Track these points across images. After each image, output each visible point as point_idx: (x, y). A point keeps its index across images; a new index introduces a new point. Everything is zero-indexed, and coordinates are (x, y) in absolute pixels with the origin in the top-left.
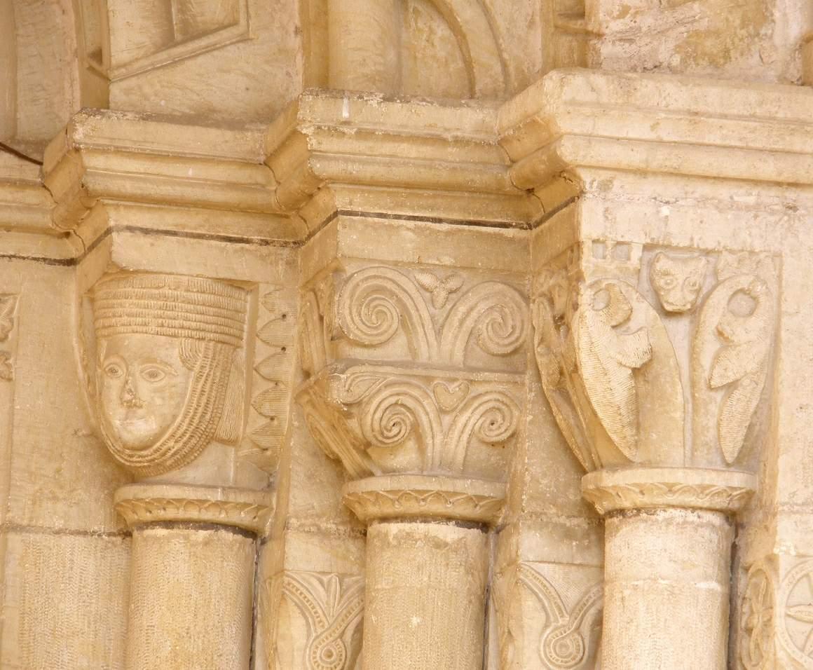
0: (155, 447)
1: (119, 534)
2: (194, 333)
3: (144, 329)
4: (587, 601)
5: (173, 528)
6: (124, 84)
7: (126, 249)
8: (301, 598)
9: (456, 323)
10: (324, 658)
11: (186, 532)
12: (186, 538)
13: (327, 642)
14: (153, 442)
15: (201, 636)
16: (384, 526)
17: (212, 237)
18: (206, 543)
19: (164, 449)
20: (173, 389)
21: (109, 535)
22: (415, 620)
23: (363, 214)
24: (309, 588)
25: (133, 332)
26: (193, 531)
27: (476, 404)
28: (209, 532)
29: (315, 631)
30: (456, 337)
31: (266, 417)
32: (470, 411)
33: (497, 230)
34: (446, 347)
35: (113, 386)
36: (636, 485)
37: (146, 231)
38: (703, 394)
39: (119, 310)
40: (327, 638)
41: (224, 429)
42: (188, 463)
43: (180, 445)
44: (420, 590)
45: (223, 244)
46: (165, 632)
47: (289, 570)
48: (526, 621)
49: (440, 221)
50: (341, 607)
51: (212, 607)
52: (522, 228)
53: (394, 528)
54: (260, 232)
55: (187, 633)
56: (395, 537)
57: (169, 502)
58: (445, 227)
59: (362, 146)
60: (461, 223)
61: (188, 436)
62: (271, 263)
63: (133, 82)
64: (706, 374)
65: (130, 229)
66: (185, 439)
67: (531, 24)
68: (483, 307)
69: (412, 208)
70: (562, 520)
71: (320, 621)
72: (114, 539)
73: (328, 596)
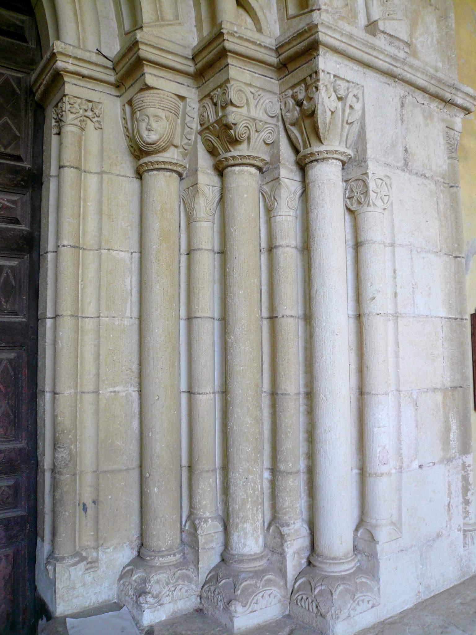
6: (148, 29)
7: (150, 80)
12: (164, 174)
14: (157, 142)
16: (233, 168)
17: (174, 81)
18: (170, 176)
23: (236, 66)
30: (260, 109)
35: (143, 125)
36: (326, 151)
37: (155, 76)
38: (345, 124)
39: (146, 101)
41: (175, 143)
49: (256, 73)
53: (237, 168)
56: (238, 171)
57: (160, 162)
58: (257, 75)
59: (239, 41)
63: (150, 29)
64: (346, 119)
65: (150, 74)
67: (275, 22)
68: (267, 101)
70: (290, 166)
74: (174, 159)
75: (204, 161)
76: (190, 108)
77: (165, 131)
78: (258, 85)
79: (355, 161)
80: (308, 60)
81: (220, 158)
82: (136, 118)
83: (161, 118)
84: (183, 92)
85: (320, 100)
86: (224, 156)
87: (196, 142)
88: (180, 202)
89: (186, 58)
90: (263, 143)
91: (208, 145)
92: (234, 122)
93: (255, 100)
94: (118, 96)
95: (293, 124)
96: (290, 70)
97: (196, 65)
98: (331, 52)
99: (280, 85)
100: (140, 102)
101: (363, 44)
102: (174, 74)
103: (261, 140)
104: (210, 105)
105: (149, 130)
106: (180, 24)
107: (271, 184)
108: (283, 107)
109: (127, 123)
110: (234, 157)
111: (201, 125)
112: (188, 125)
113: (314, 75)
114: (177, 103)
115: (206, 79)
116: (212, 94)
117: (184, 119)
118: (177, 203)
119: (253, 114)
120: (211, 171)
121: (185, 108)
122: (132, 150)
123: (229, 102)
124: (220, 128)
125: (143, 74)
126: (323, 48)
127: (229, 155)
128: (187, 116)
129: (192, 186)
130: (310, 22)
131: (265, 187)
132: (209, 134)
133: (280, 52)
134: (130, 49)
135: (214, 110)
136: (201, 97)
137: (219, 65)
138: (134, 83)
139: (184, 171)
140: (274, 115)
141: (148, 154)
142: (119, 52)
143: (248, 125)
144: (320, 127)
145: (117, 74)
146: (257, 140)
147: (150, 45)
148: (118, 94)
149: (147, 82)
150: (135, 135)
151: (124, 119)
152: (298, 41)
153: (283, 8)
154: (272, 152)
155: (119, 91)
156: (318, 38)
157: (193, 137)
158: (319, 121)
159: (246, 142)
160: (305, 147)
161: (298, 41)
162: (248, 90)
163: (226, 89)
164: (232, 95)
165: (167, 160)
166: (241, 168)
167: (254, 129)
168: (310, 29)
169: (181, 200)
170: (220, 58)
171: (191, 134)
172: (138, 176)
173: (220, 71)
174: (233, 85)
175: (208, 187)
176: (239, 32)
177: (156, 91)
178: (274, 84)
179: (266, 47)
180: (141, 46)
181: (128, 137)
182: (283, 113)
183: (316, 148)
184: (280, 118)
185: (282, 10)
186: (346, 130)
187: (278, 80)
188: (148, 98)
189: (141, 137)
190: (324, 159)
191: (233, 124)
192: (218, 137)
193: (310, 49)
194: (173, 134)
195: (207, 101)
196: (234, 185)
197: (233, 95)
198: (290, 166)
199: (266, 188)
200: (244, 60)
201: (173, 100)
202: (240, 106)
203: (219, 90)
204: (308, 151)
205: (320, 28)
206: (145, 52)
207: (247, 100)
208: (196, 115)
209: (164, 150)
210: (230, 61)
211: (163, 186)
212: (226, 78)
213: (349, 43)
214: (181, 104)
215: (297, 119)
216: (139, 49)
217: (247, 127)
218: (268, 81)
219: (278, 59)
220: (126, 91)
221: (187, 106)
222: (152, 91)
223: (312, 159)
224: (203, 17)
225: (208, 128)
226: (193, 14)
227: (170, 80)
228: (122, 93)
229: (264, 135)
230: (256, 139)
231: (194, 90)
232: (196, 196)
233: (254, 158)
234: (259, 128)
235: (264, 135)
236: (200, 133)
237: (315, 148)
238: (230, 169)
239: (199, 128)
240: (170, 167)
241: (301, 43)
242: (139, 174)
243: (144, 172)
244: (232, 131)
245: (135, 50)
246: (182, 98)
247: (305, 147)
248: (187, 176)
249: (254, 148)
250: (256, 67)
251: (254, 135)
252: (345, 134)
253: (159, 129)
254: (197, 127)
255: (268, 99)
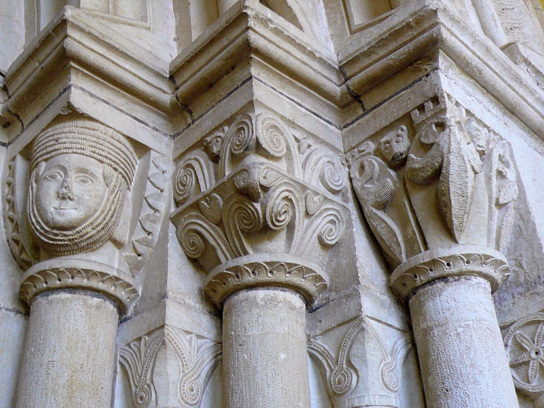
0: (77, 230)
1: (13, 311)
2: (113, 164)
3: (82, 151)
4: (397, 348)
5: (75, 294)
8: (175, 346)
9: (312, 164)
10: (188, 391)
11: (85, 297)
12: (85, 302)
13: (191, 380)
14: (79, 224)
15: (91, 371)
16: (252, 293)
17: (128, 114)
19: (84, 232)
20: (97, 192)
21: (7, 310)
22: (283, 356)
24: (180, 340)
25: (74, 153)
26: (90, 297)
27: (325, 214)
28: (101, 300)
29: (183, 371)
31: (146, 231)
32: (321, 218)
33: (326, 123)
34: (307, 176)
35: (51, 188)
37: (92, 95)
40: (191, 377)
42: (94, 250)
43: (95, 232)
44: (283, 336)
45: (134, 120)
46: (64, 366)
47: (168, 325)
48: (368, 356)
49: (301, 106)
50: (198, 357)
51: (99, 352)
52: (337, 128)
53: (261, 294)
54: (154, 122)
55: (82, 368)
56: (263, 299)
57: (79, 272)
60: (310, 111)
61: (101, 226)
62: (158, 141)
65: (82, 89)
66: (99, 228)
67: (327, 41)
68: (325, 159)
69: (288, 92)
71: (186, 365)
72: (9, 313)
73: (191, 348)
74: (113, 268)
75: (181, 281)
76: (157, 171)
77: (99, 204)
78: (307, 127)
79: (518, 285)
80: (410, 82)
81: (222, 269)
82: (37, 174)
83: (92, 174)
84: (144, 136)
85: (454, 146)
86: (232, 263)
87: (164, 239)
88: (115, 372)
89: (158, 75)
90: (317, 244)
91: (193, 244)
92: (264, 183)
93: (302, 154)
94: (4, 145)
95: (383, 206)
96: (368, 106)
97: (177, 89)
98: (457, 70)
99: (344, 137)
100: (51, 143)
101: (505, 69)
102: (130, 100)
103: (315, 236)
104: (202, 161)
105: (63, 198)
106: (148, 29)
107: (338, 333)
108: (356, 174)
109: (13, 192)
110: (255, 267)
111: (177, 204)
112: (150, 201)
113: (430, 105)
114: (130, 155)
115: (195, 116)
116: (208, 139)
117: (142, 187)
118: (109, 373)
119: (299, 175)
120: (194, 302)
121: (146, 168)
122: (16, 249)
123: (252, 143)
124: (225, 203)
125: (67, 89)
126: (444, 57)
127: (243, 261)
128: (149, 183)
129: (149, 334)
130: (418, 8)
131: (319, 342)
132: (198, 217)
133: (348, 74)
134: (46, 40)
135: (212, 170)
136: (182, 150)
137: (227, 83)
138: (41, 113)
139: (132, 300)
140: (338, 189)
141: (54, 251)
142: (21, 56)
143: (291, 196)
144: (453, 203)
145: (10, 98)
146: (307, 233)
147: (91, 35)
148: (6, 141)
149: (71, 100)
150: (29, 210)
151: (9, 184)
152: (391, 47)
153: (342, 18)
154: (334, 265)
155: (9, 134)
156: (440, 34)
157: (157, 229)
158: (452, 189)
159: (283, 235)
160: (412, 251)
161: (391, 47)
162: (290, 132)
163: (247, 121)
164: (260, 131)
165: (97, 268)
166: (271, 293)
167: (302, 209)
168: (419, 21)
169: (119, 369)
170: (233, 68)
171: (154, 222)
172: (21, 309)
173: (229, 94)
174: (259, 115)
175: (188, 337)
176: (275, 22)
177: (88, 124)
178: (334, 134)
179: (321, 61)
180: (70, 31)
181: (12, 220)
182: (357, 185)
183: (441, 249)
184: (350, 195)
185: (339, 22)
186: (495, 218)
187: (341, 129)
188: (70, 135)
189: (42, 211)
190: (460, 274)
191: (262, 186)
192: (220, 224)
193: (417, 60)
194: (115, 214)
195: (200, 155)
196: (253, 331)
197: (261, 129)
198: (378, 294)
199: (325, 344)
200: (281, 76)
201: (123, 149)
202: (276, 155)
203: (226, 128)
204: (424, 257)
205: (441, 18)
206: (76, 43)
207: (288, 148)
208: (167, 185)
209: (91, 245)
210: (254, 71)
211: (80, 330)
212: (245, 102)
213: (485, 60)
214: (138, 164)
215: (393, 195)
216: (67, 36)
217: (291, 200)
218: (322, 124)
219: (344, 86)
220: (23, 130)
221: (152, 165)
222: (80, 123)
223: (432, 274)
224: (193, 24)
225: (196, 206)
226: (172, 22)
227: (121, 111)
228: (13, 136)
229: (321, 224)
230: (305, 232)
231: (166, 139)
232: (160, 355)
233: (303, 271)
234: (312, 208)
235: (321, 224)
236: (175, 220)
237: (440, 249)
238: (243, 294)
239: (173, 209)
240: (101, 286)
241: (395, 50)
242: (25, 305)
243: (36, 294)
244: (258, 206)
245: (57, 40)
246: (141, 149)
247: (412, 251)
248: (136, 313)
249: (297, 250)
250: (301, 94)
251: (301, 222)
252: (495, 226)
253: (87, 197)
254: (169, 207)
255: (326, 156)
